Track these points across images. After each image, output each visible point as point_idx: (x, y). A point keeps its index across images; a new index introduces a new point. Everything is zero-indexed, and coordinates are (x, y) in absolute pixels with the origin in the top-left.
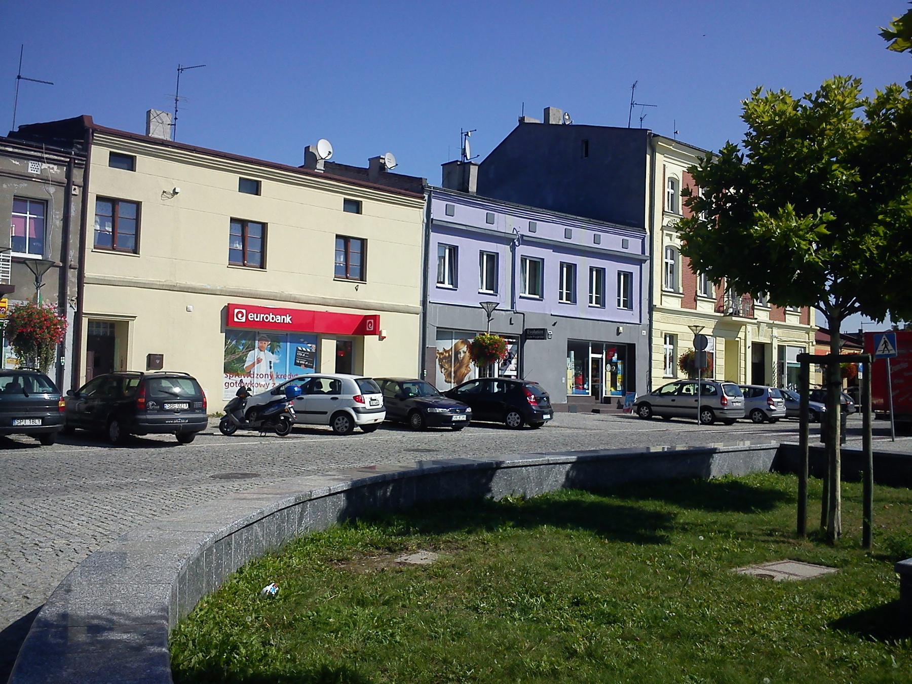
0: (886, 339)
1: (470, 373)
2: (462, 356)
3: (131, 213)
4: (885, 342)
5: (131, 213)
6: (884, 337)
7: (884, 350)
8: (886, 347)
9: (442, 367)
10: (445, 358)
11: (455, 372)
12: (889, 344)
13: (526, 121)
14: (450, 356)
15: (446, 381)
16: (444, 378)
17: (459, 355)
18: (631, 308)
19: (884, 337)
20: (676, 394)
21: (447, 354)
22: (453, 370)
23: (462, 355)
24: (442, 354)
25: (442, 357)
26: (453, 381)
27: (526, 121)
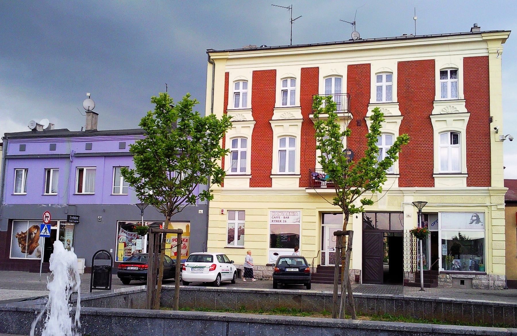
0: (47, 227)
1: (38, 247)
2: (33, 236)
3: (303, 69)
4: (46, 229)
5: (303, 69)
6: (46, 226)
7: (44, 233)
8: (46, 231)
9: (20, 243)
10: (22, 237)
11: (28, 246)
12: (48, 230)
13: (293, 250)
14: (25, 236)
15: (22, 252)
16: (21, 250)
17: (31, 236)
18: (442, 240)
19: (46, 226)
20: (364, 220)
21: (24, 235)
22: (27, 245)
23: (34, 235)
24: (20, 235)
25: (20, 237)
26: (26, 252)
27: (293, 250)
